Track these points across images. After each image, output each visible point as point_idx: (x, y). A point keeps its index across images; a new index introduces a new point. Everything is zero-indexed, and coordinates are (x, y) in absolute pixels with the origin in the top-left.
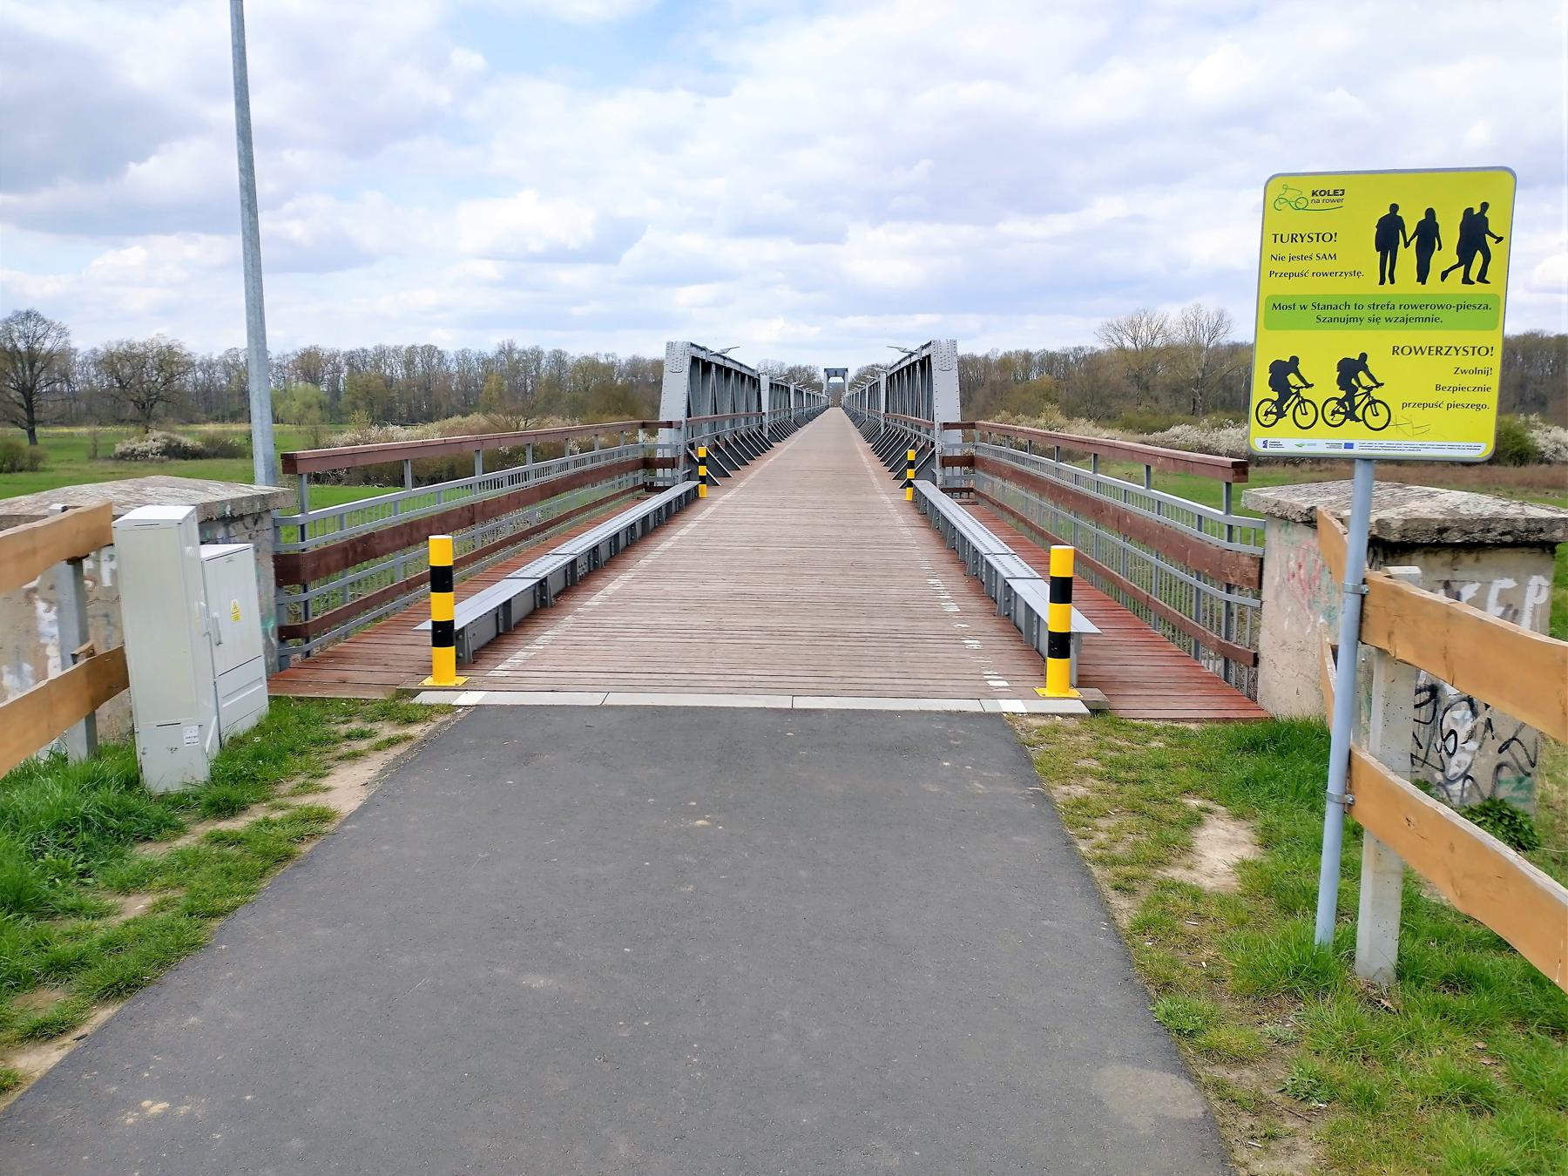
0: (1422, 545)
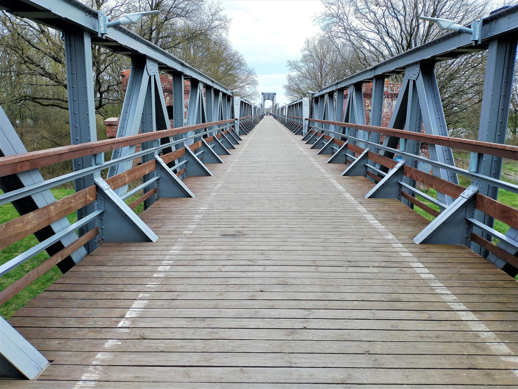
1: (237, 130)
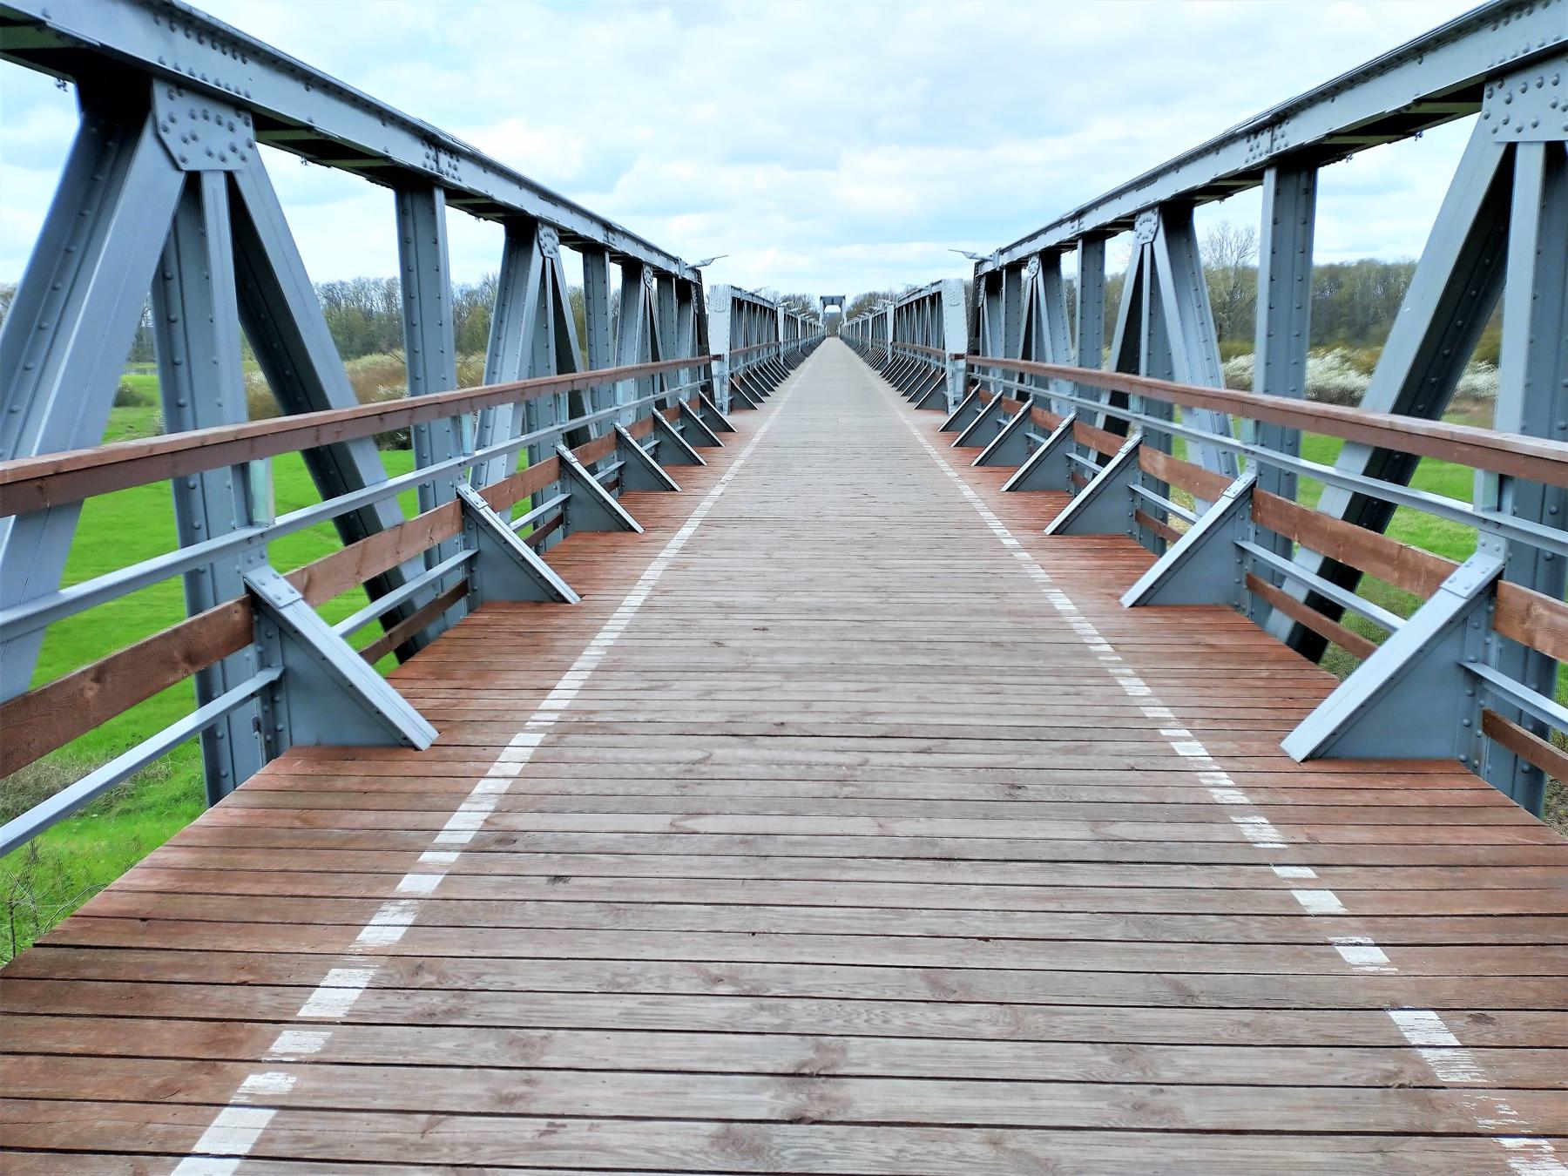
0: (1439, 762)
1: (722, 394)
